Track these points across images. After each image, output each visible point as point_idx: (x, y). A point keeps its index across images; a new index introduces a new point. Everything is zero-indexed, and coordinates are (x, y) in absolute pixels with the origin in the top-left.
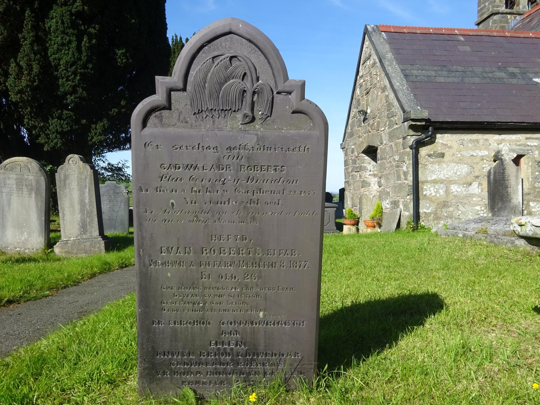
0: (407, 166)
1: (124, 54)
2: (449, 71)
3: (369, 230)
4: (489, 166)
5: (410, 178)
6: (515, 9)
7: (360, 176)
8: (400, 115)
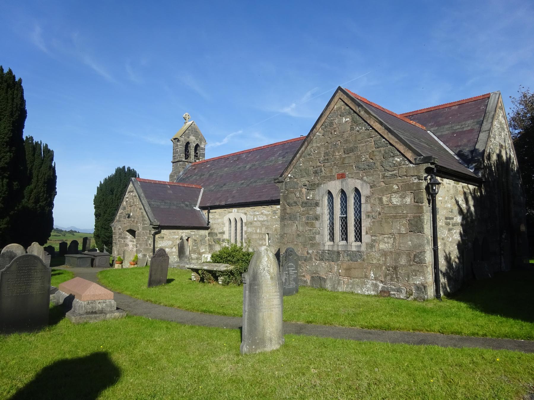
0: (151, 241)
1: (17, 185)
2: (165, 203)
3: (132, 266)
4: (178, 242)
5: (152, 246)
6: (189, 160)
7: (124, 241)
8: (148, 222)
